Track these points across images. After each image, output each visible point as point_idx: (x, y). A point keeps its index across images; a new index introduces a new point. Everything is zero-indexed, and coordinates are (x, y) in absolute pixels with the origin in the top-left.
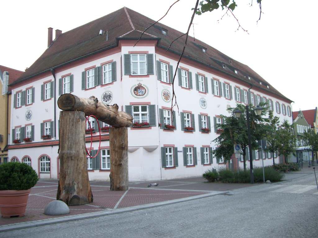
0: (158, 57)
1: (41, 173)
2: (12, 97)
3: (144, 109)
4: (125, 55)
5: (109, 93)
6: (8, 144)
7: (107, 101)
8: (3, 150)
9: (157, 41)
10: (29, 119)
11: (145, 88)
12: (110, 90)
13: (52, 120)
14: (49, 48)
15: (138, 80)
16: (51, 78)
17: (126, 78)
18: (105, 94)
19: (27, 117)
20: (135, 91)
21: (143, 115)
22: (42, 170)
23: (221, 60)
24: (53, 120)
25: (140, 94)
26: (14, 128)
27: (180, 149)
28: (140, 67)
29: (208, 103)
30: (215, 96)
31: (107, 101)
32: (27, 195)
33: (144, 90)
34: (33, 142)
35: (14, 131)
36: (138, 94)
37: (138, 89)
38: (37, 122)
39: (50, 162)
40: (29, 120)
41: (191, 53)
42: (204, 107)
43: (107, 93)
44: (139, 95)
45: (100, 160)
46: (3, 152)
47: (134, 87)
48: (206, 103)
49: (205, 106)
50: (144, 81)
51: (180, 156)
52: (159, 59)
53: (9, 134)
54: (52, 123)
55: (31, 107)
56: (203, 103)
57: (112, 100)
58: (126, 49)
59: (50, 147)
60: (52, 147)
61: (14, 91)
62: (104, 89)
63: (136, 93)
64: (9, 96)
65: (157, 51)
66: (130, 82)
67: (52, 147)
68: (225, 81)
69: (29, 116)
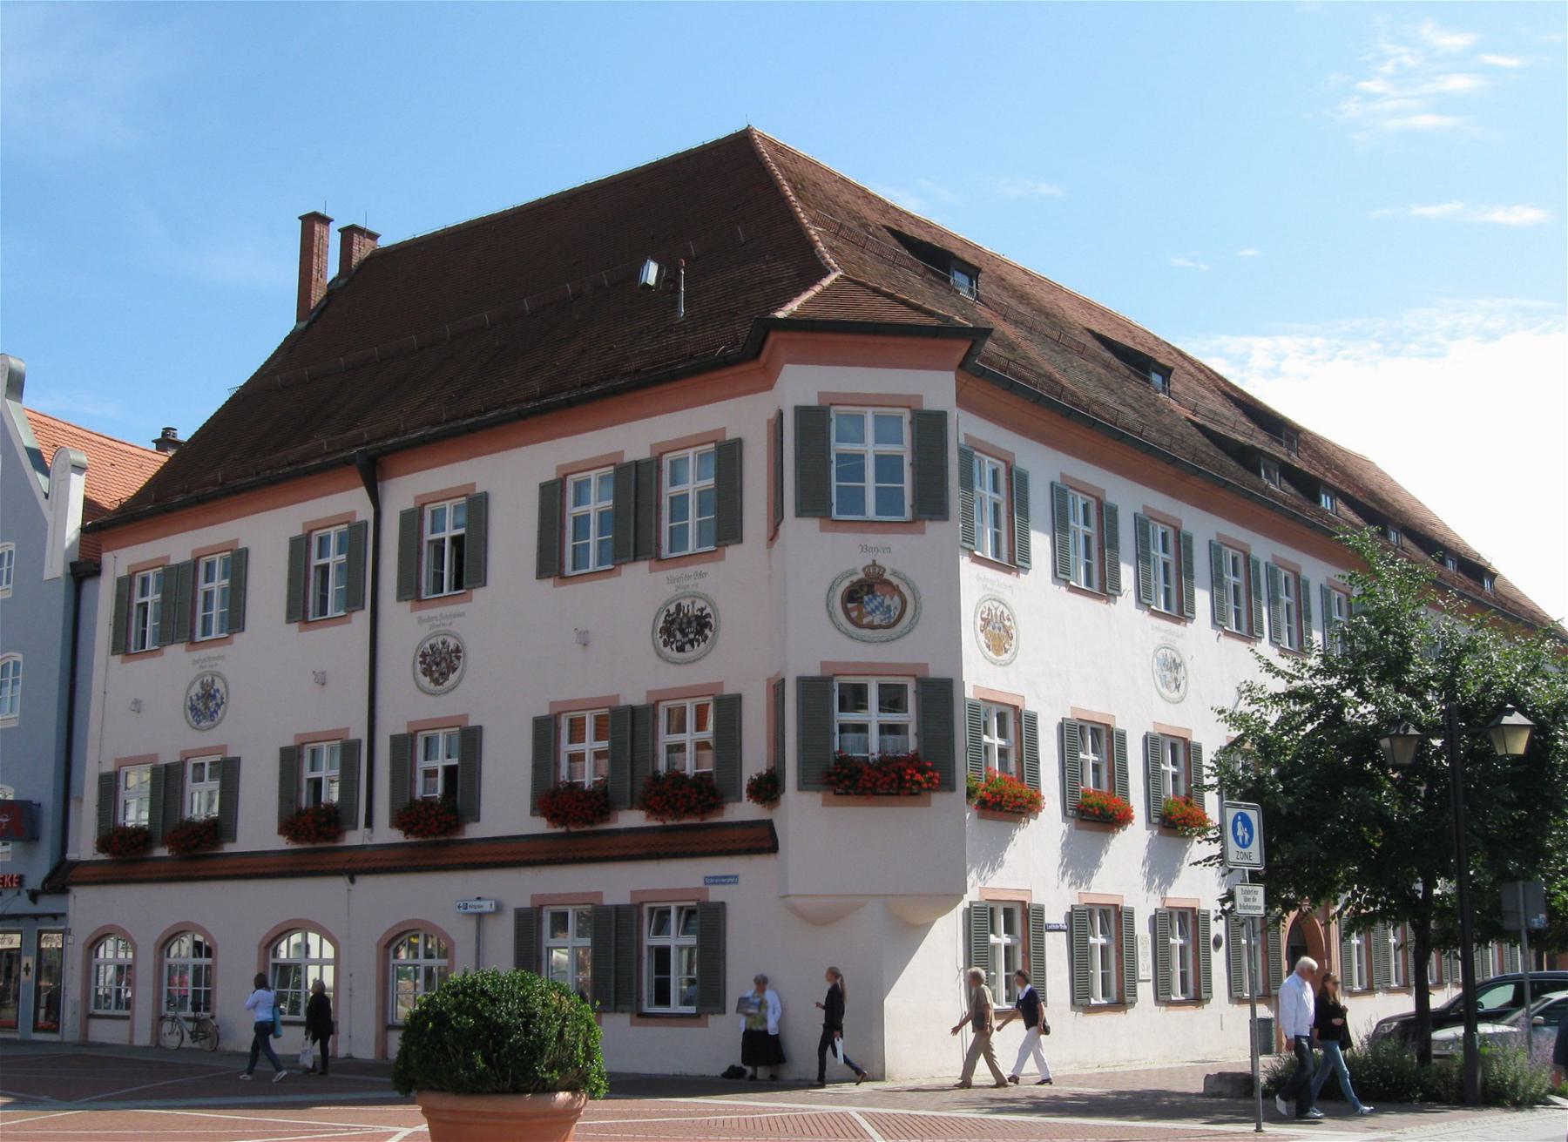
0: (965, 427)
1: (91, 1016)
2: (103, 595)
3: (892, 699)
4: (801, 412)
5: (699, 604)
6: (72, 856)
7: (688, 647)
8: (38, 887)
9: (963, 347)
10: (204, 724)
11: (903, 588)
12: (703, 586)
13: (353, 736)
14: (308, 328)
15: (864, 548)
16: (352, 502)
17: (800, 531)
18: (672, 609)
19: (193, 708)
20: (850, 605)
21: (886, 729)
22: (97, 1006)
23: (1243, 432)
24: (359, 732)
25: (877, 619)
26: (109, 767)
27: (1055, 915)
28: (878, 480)
29: (1025, 630)
30: (1227, 633)
31: (688, 647)
32: (1214, 1096)
33: (896, 598)
34: (229, 848)
35: (110, 786)
36: (865, 621)
37: (865, 596)
38: (254, 738)
39: (215, 961)
40: (209, 728)
41: (1104, 397)
42: (1175, 695)
43: (685, 603)
44: (872, 627)
45: (640, 958)
46: (34, 896)
47: (846, 584)
48: (1182, 672)
49: (1178, 687)
50: (899, 553)
51: (1056, 949)
52: (1062, 475)
53: (80, 800)
54: (349, 751)
55: (221, 657)
56: (1170, 669)
57: (713, 645)
58: (801, 383)
59: (341, 883)
60: (352, 881)
61: (118, 562)
62: (671, 580)
63: (854, 614)
64: (88, 586)
65: (963, 401)
66: (822, 555)
67: (352, 881)
68: (1278, 554)
69: (206, 704)
